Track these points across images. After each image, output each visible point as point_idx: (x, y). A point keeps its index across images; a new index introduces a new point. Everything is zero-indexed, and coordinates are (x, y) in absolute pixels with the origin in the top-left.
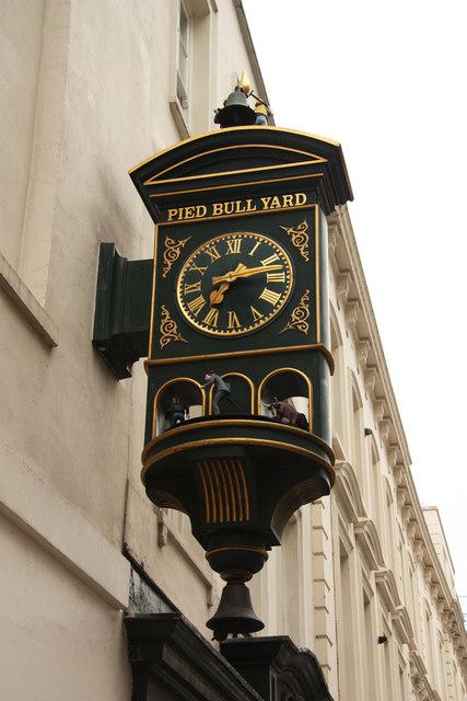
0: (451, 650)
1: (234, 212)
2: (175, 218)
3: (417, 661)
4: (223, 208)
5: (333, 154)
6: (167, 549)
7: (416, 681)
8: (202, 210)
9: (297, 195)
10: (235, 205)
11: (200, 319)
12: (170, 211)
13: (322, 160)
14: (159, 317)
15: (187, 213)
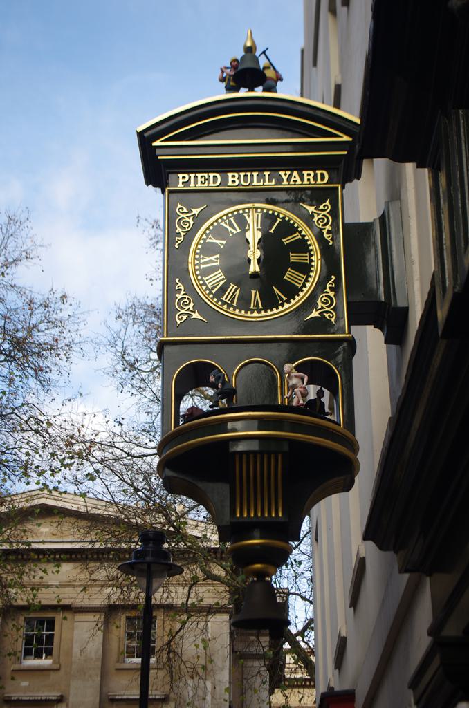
4: (239, 178)
10: (252, 176)
13: (346, 138)
15: (199, 180)
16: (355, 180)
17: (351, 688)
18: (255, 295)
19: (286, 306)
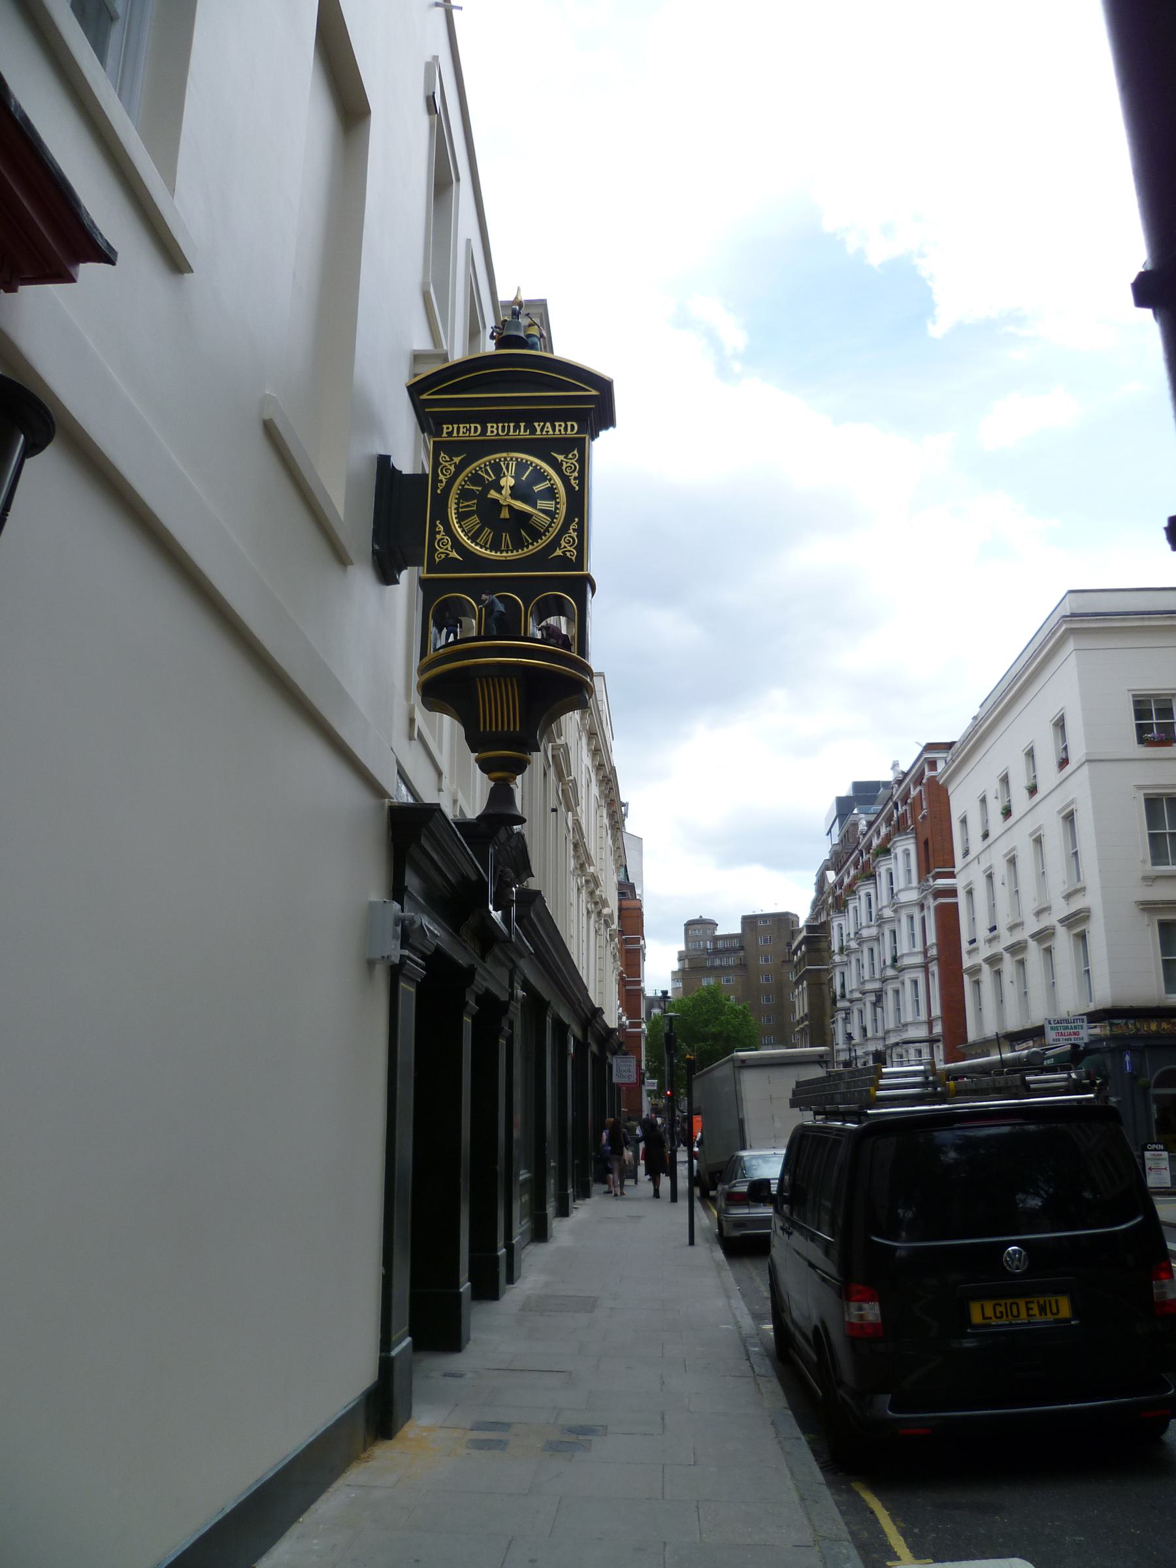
0: (605, 815)
1: (507, 434)
2: (450, 434)
3: (577, 823)
5: (604, 387)
6: (416, 744)
7: (576, 846)
8: (476, 428)
9: (569, 424)
11: (474, 539)
12: (445, 426)
13: (594, 393)
14: (433, 533)
16: (603, 450)
17: (475, 1303)
18: (506, 537)
19: (531, 547)
